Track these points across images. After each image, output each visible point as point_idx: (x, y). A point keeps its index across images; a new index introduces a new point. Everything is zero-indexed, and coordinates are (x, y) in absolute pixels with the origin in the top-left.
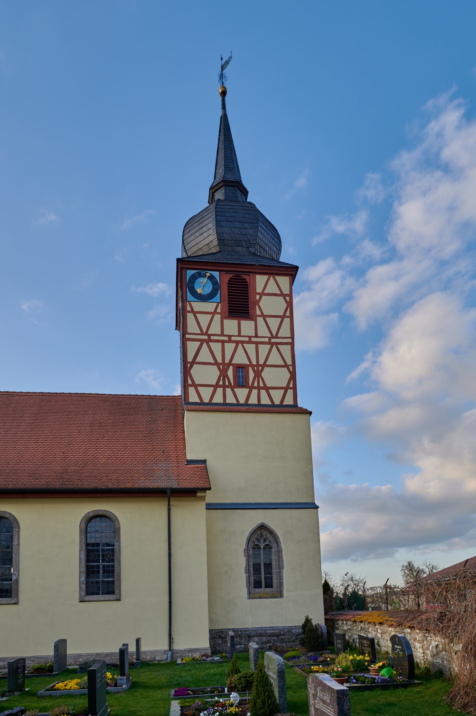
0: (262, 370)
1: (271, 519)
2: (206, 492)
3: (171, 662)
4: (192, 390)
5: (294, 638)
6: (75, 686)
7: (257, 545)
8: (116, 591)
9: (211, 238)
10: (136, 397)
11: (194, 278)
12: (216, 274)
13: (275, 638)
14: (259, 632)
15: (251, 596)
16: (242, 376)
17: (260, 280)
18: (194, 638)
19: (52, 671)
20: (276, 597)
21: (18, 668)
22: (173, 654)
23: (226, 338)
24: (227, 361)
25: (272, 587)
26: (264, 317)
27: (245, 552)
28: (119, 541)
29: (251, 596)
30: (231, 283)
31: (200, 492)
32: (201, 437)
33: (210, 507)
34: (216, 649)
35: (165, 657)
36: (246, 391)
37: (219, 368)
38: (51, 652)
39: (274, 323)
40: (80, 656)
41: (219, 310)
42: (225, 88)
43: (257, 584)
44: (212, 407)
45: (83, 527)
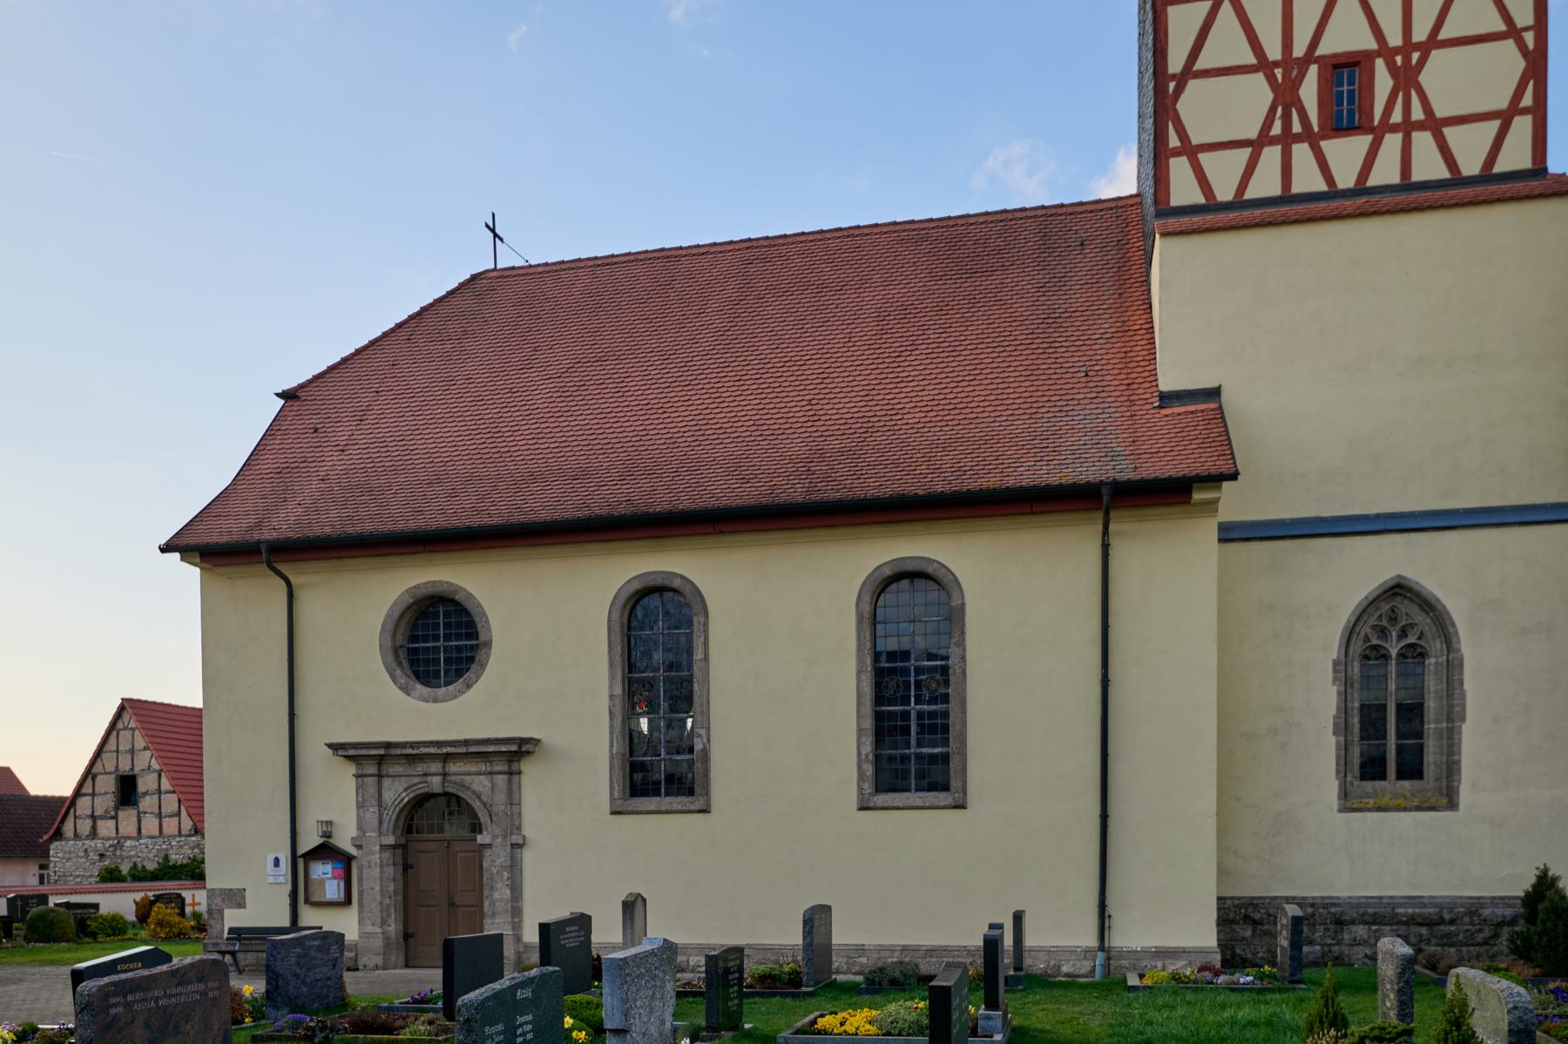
0: (1422, 61)
1: (1424, 561)
2: (1220, 488)
3: (1109, 978)
4: (1179, 168)
5: (1487, 933)
6: (868, 1027)
7: (1375, 647)
8: (953, 783)
10: (1004, 216)
13: (1424, 931)
14: (1370, 911)
15: (1349, 802)
16: (1351, 93)
18: (1173, 920)
19: (799, 984)
20: (1433, 809)
21: (727, 971)
22: (1109, 959)
24: (1299, 50)
25: (1421, 777)
27: (1335, 671)
28: (962, 644)
29: (1349, 802)
31: (1200, 489)
32: (1206, 314)
33: (1231, 534)
34: (1233, 952)
35: (1086, 966)
36: (1363, 142)
37: (1271, 79)
38: (796, 938)
40: (861, 950)
43: (1373, 768)
44: (1302, 208)
45: (867, 608)
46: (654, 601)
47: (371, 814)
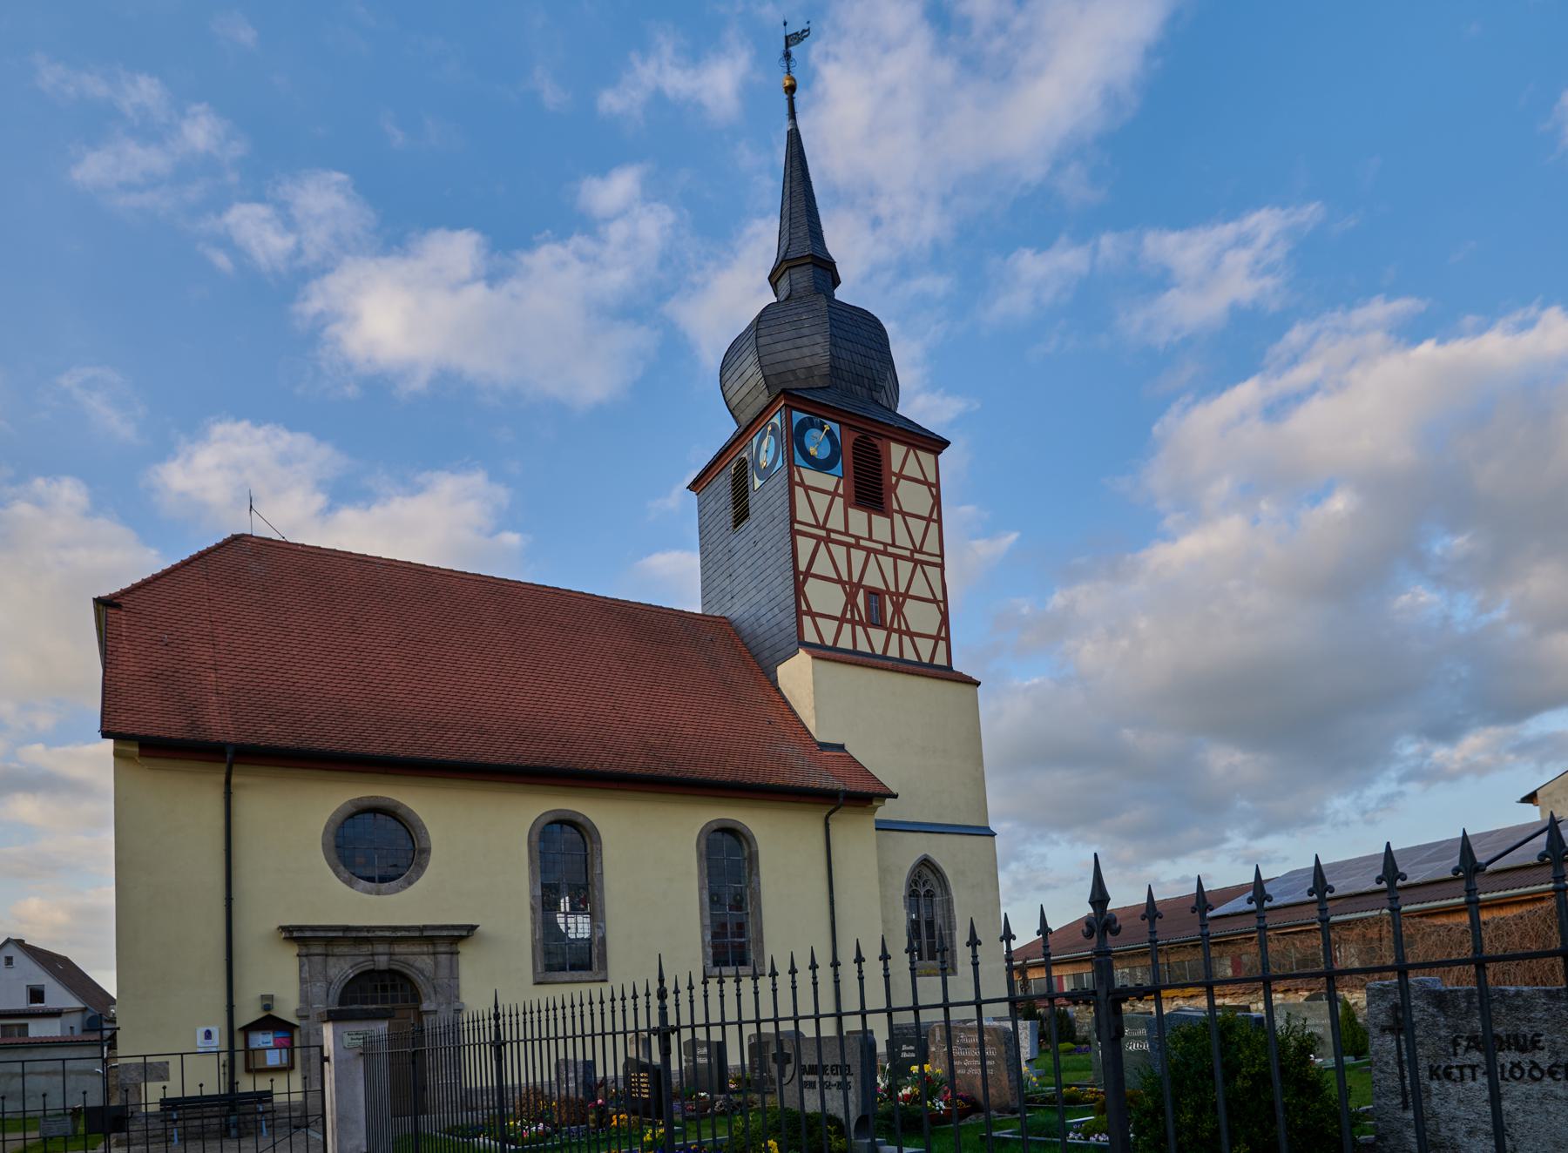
1: (942, 850)
9: (817, 360)
11: (803, 427)
12: (836, 427)
17: (897, 451)
23: (852, 541)
24: (855, 579)
26: (904, 514)
30: (856, 446)
33: (884, 827)
39: (917, 527)
41: (841, 491)
42: (793, 79)
46: (570, 834)
47: (318, 989)
